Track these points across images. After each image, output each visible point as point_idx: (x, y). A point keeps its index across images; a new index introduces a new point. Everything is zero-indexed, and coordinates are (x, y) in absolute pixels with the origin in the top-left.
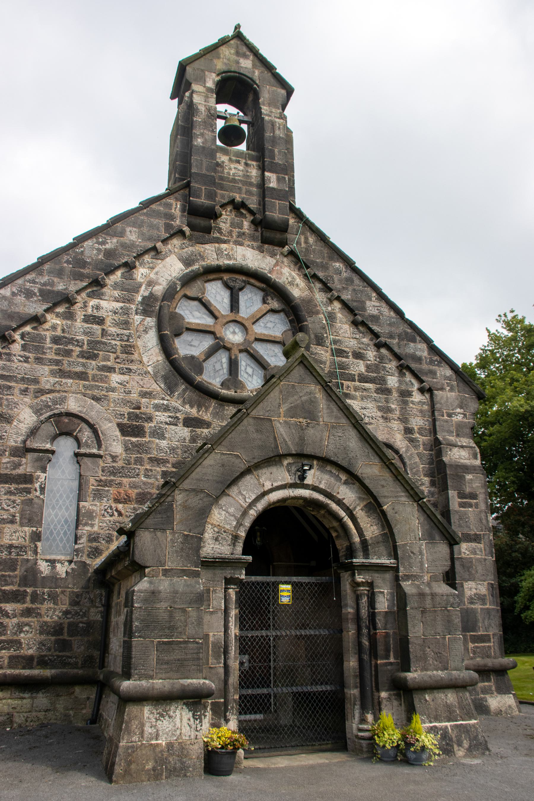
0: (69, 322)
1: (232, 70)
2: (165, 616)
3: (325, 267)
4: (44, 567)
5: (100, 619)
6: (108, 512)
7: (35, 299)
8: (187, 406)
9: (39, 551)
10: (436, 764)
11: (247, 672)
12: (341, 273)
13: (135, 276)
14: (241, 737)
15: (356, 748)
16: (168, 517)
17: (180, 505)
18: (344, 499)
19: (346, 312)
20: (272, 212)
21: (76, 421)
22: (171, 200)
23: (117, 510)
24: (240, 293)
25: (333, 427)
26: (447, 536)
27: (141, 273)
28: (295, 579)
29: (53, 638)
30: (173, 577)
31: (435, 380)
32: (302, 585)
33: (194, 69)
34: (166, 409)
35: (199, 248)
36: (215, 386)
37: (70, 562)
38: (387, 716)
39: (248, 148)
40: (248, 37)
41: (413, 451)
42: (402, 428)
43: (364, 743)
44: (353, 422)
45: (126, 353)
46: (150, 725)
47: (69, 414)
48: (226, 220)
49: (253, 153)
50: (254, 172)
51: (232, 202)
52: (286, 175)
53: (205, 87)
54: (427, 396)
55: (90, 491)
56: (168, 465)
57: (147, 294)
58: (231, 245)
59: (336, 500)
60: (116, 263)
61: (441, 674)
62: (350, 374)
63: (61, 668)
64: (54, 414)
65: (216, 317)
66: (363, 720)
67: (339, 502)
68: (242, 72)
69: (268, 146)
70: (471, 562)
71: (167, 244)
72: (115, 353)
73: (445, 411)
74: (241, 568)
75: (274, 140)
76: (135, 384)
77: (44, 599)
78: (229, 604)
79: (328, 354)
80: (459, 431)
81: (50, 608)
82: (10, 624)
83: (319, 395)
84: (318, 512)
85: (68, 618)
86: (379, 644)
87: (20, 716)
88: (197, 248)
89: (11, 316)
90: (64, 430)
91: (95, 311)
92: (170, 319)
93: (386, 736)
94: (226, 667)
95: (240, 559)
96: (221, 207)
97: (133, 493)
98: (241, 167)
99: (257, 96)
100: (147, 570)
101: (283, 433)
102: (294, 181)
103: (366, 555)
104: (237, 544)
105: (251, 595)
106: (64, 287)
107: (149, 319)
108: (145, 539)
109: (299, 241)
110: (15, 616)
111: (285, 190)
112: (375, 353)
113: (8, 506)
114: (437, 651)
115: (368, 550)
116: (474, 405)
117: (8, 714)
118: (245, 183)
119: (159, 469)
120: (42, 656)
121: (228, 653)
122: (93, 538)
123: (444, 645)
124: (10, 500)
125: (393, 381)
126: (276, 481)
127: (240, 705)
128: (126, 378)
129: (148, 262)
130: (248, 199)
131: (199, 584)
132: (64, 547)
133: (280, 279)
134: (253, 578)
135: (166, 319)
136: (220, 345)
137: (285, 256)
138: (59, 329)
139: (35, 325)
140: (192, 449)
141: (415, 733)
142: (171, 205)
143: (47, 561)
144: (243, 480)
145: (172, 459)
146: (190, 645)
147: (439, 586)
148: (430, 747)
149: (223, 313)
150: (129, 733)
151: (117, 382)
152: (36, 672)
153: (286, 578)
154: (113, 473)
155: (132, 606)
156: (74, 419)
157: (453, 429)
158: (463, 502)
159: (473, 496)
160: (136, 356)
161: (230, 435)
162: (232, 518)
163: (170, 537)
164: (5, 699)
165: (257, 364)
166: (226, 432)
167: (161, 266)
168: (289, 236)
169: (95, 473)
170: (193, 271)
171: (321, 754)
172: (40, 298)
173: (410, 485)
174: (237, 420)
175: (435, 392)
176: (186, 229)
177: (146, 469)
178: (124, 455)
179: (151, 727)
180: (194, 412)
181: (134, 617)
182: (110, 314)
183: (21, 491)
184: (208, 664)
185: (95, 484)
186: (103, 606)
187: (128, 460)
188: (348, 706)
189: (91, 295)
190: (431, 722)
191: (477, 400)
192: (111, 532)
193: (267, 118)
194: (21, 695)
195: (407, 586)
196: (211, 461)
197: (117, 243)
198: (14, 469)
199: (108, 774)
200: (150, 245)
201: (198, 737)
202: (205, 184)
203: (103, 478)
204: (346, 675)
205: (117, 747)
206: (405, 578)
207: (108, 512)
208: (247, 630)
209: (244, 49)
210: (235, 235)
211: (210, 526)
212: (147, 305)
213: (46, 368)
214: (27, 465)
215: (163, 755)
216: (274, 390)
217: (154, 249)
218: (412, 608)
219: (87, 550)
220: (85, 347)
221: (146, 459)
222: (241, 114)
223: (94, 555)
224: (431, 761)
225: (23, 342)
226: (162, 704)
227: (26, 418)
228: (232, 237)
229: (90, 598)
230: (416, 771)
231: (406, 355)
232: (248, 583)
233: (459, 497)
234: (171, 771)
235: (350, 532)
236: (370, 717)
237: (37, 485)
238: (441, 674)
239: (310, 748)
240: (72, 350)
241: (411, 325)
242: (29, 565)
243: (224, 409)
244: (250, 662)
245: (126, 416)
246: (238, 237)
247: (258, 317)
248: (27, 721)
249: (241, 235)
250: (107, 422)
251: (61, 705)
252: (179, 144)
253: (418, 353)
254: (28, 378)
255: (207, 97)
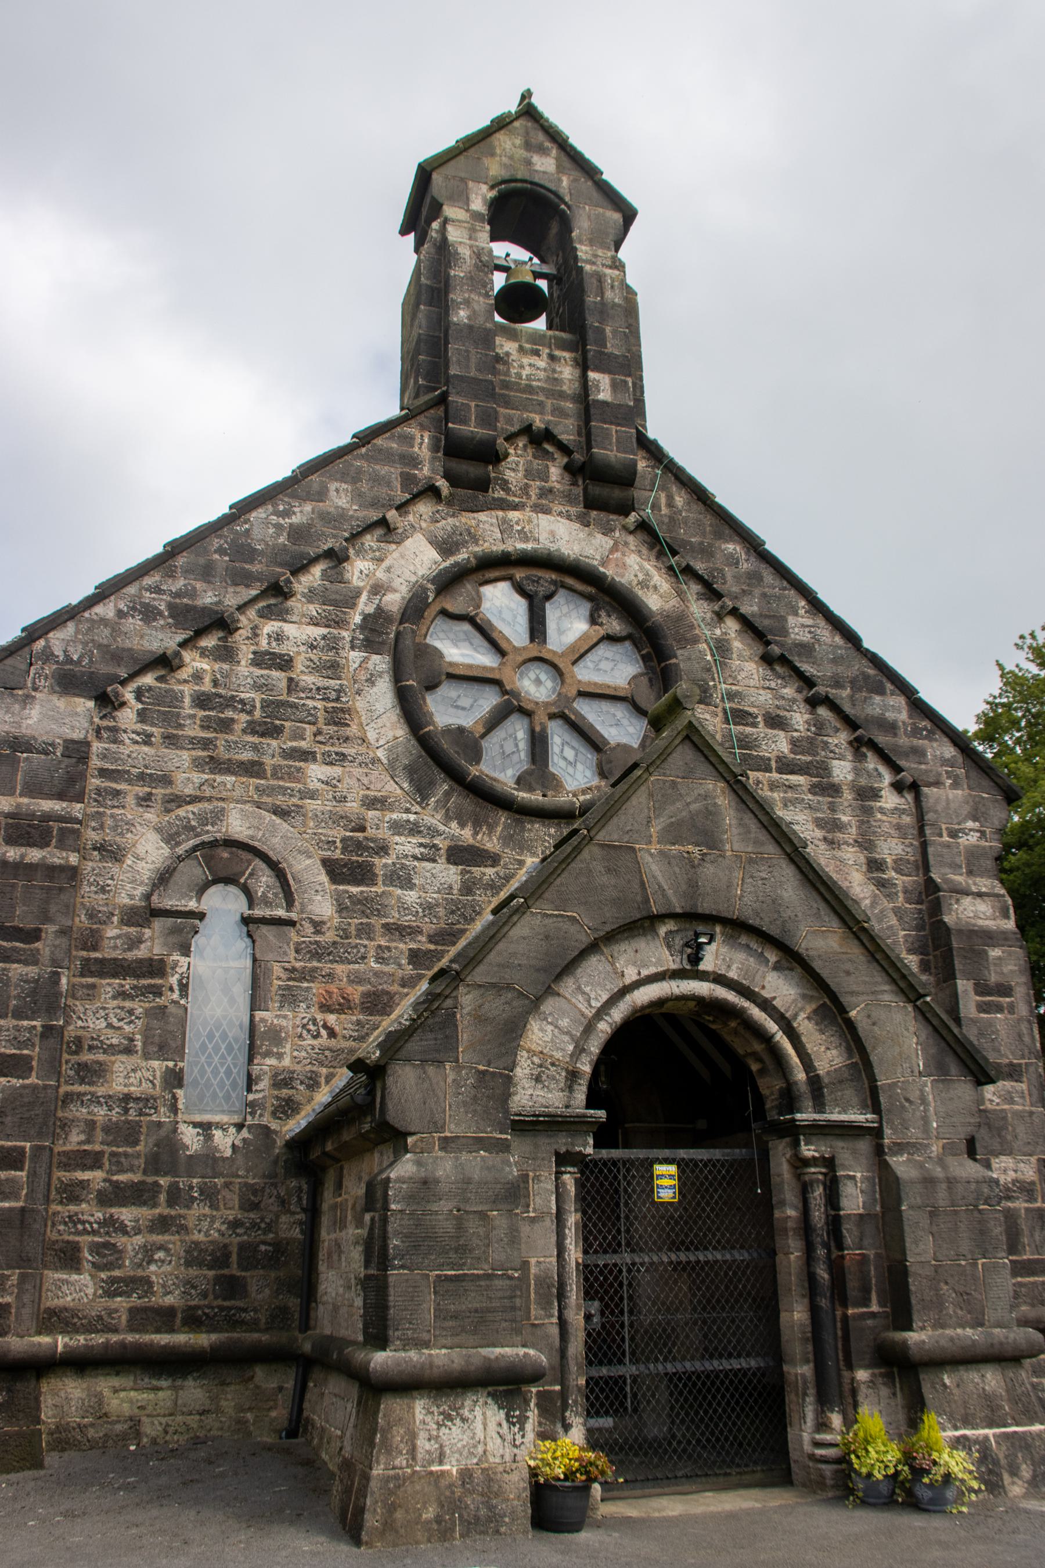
0: (226, 666)
1: (519, 177)
2: (448, 1226)
3: (707, 552)
4: (190, 1138)
5: (300, 1236)
6: (309, 1031)
7: (162, 622)
8: (454, 824)
9: (180, 1106)
10: (973, 1511)
11: (599, 1334)
12: (737, 563)
13: (347, 576)
14: (598, 1458)
15: (810, 1481)
16: (446, 1037)
17: (469, 1014)
18: (774, 998)
19: (749, 638)
20: (605, 449)
21: (245, 855)
22: (411, 429)
23: (325, 1026)
24: (547, 605)
25: (751, 861)
26: (972, 1066)
27: (359, 570)
28: (682, 1153)
29: (211, 1273)
30: (460, 1152)
31: (923, 767)
32: (696, 1165)
33: (446, 178)
34: (414, 829)
35: (467, 519)
36: (506, 784)
37: (240, 1126)
38: (872, 1416)
39: (550, 326)
40: (546, 115)
41: (886, 904)
42: (862, 859)
43: (828, 1469)
44: (789, 850)
45: (336, 724)
46: (427, 1436)
47: (231, 843)
48: (516, 465)
49: (563, 335)
50: (567, 372)
51: (527, 430)
52: (629, 375)
53: (468, 210)
54: (910, 797)
55: (274, 989)
56: (420, 938)
57: (370, 609)
58: (528, 513)
59: (759, 1001)
60: (312, 552)
61: (970, 1333)
62: (762, 758)
63: (227, 1331)
64: (203, 843)
65: (501, 652)
66: (823, 1426)
67: (766, 1005)
68: (536, 180)
69: (592, 321)
70: (1005, 1118)
71: (407, 513)
72: (314, 724)
73: (944, 827)
74: (587, 1133)
75: (604, 310)
76: (355, 783)
77: (193, 1199)
78: (564, 1202)
79: (718, 720)
80: (973, 862)
81: (204, 1215)
82: (130, 1248)
83: (723, 800)
84: (725, 1024)
85: (237, 1235)
86: (849, 1277)
87: (153, 1423)
88: (463, 520)
89: (116, 656)
90: (222, 874)
91: (274, 644)
92: (416, 656)
93: (873, 1454)
94: (563, 1323)
95: (585, 1116)
96: (507, 439)
97: (356, 993)
98: (542, 364)
99: (566, 225)
100: (410, 1140)
101: (658, 874)
102: (642, 387)
103: (820, 1105)
104: (576, 1087)
105: (602, 1185)
106: (215, 599)
107: (376, 658)
108: (405, 1082)
109: (657, 502)
110: (138, 1231)
111: (628, 406)
112: (807, 716)
113: (120, 1020)
114: (962, 1289)
115: (822, 1095)
116: (997, 813)
117: (131, 1419)
118: (551, 394)
119: (403, 947)
120: (190, 1308)
121: (566, 1297)
122: (282, 1081)
123: (975, 1278)
124: (122, 1008)
125: (842, 770)
126: (646, 966)
127: (588, 1398)
128: (336, 771)
129: (371, 548)
130: (557, 424)
131: (510, 1166)
132: (227, 1097)
133: (623, 576)
134: (604, 1153)
135: (408, 656)
136: (512, 707)
137: (631, 533)
138: (207, 679)
139: (162, 672)
140: (464, 906)
141: (930, 1448)
142: (412, 438)
143: (196, 1125)
144: (585, 964)
145: (429, 927)
146: (496, 1282)
147: (961, 1165)
148: (960, 1476)
149: (516, 644)
150: (389, 1452)
151: (319, 780)
152: (181, 1338)
153: (667, 1153)
154: (317, 955)
155: (386, 1208)
156: (240, 852)
157: (961, 860)
158: (985, 1003)
159: (1004, 990)
160: (353, 730)
161: (559, 880)
162: (566, 1038)
163: (451, 1077)
164: (124, 1390)
165: (584, 742)
166: (552, 873)
167: (395, 555)
168: (638, 494)
169: (283, 954)
170: (457, 564)
171: (743, 1492)
172: (170, 620)
173: (898, 970)
174: (568, 850)
175: (925, 790)
176: (442, 483)
177: (380, 946)
178: (337, 920)
179: (429, 1440)
180: (466, 835)
181: (390, 1229)
182: (303, 648)
183: (144, 992)
184: (529, 1318)
185: (284, 976)
186: (304, 1210)
187: (344, 930)
188: (790, 1398)
189: (266, 614)
190: (956, 1428)
191: (1004, 804)
192: (315, 1069)
193: (588, 268)
194: (155, 1382)
195: (898, 1163)
196: (525, 930)
197: (313, 512)
198: (130, 949)
199: (351, 1528)
200: (375, 516)
201: (518, 1458)
202: (475, 397)
203: (298, 965)
204: (784, 1338)
205: (366, 1478)
206: (895, 1148)
207: (309, 1031)
208: (596, 1252)
209: (541, 137)
210: (533, 493)
211: (525, 1054)
212: (372, 630)
213: (185, 755)
214: (153, 942)
215: (453, 1493)
216: (639, 793)
217: (383, 522)
218: (911, 1207)
219: (271, 1103)
220: (258, 713)
221: (378, 928)
222: (536, 260)
223: (284, 1112)
224: (963, 1504)
225: (140, 706)
226: (448, 1396)
227: (149, 851)
228: (529, 497)
229: (278, 1196)
230: (936, 1522)
231: (866, 720)
232: (595, 1162)
233: (977, 993)
234: (470, 1523)
235: (787, 1062)
236: (836, 1420)
237: (174, 980)
238: (970, 1333)
239: (721, 1479)
240: (232, 720)
241: (875, 661)
242: (163, 1132)
243: (523, 829)
244: (602, 1313)
245: (338, 844)
246: (540, 496)
247: (582, 651)
248: (166, 1432)
249: (546, 493)
250: (303, 857)
251: (230, 1399)
252: (424, 323)
253: (890, 715)
254: (151, 775)
255: (472, 230)
